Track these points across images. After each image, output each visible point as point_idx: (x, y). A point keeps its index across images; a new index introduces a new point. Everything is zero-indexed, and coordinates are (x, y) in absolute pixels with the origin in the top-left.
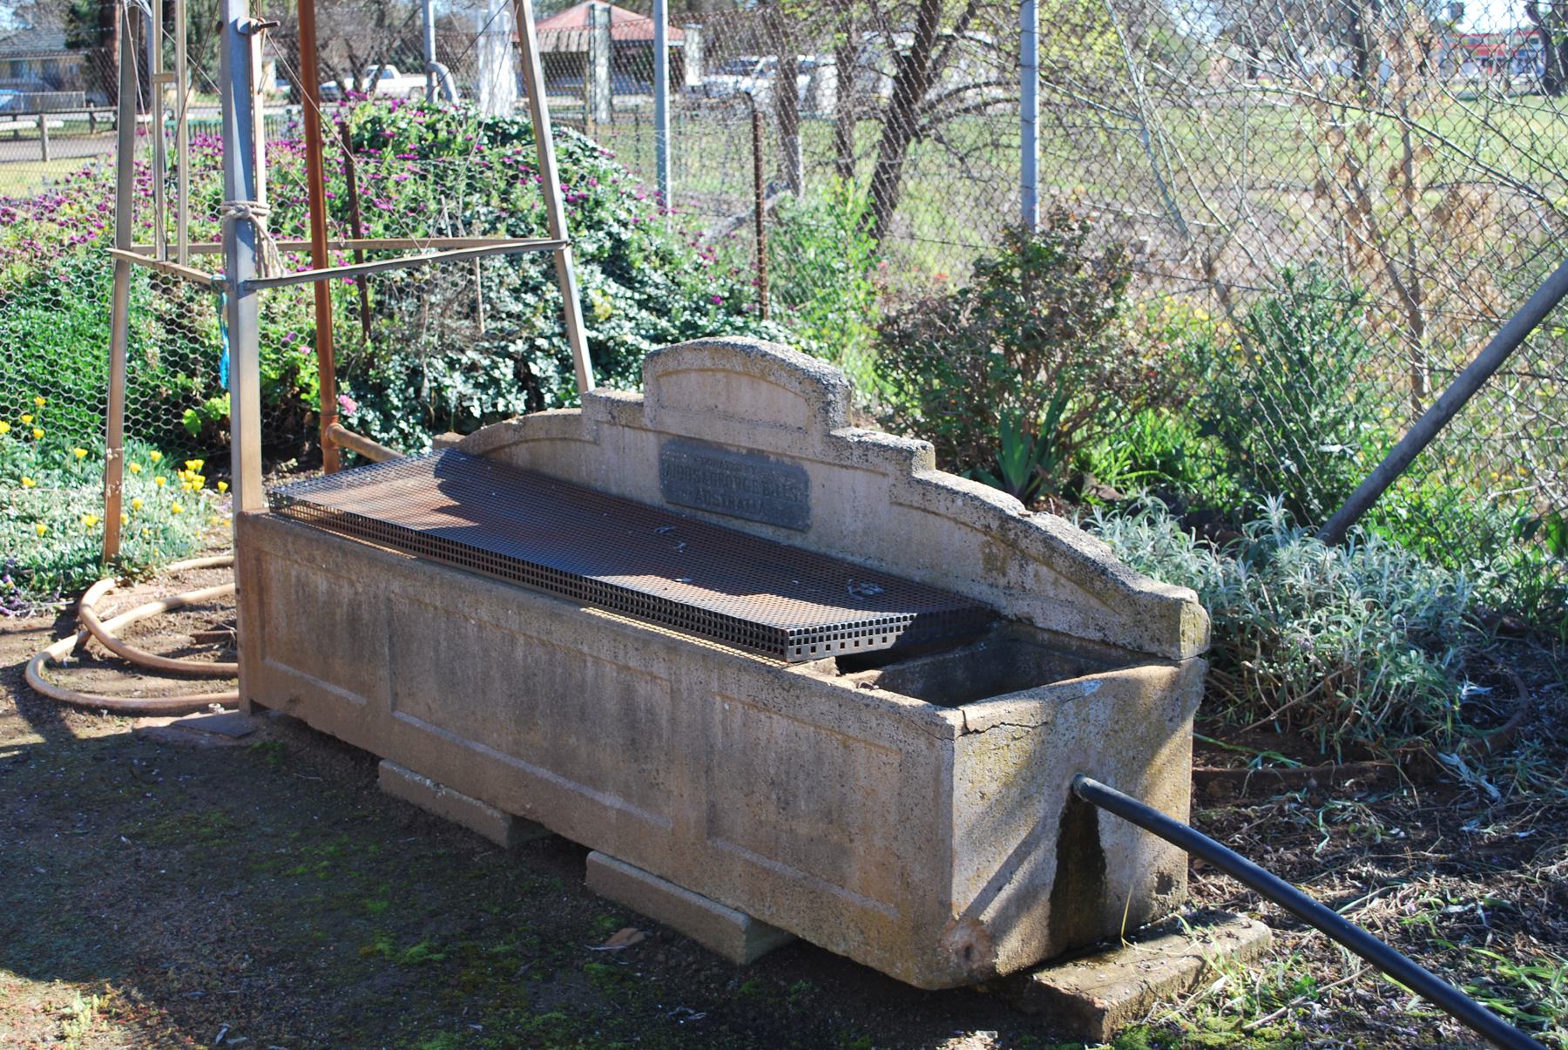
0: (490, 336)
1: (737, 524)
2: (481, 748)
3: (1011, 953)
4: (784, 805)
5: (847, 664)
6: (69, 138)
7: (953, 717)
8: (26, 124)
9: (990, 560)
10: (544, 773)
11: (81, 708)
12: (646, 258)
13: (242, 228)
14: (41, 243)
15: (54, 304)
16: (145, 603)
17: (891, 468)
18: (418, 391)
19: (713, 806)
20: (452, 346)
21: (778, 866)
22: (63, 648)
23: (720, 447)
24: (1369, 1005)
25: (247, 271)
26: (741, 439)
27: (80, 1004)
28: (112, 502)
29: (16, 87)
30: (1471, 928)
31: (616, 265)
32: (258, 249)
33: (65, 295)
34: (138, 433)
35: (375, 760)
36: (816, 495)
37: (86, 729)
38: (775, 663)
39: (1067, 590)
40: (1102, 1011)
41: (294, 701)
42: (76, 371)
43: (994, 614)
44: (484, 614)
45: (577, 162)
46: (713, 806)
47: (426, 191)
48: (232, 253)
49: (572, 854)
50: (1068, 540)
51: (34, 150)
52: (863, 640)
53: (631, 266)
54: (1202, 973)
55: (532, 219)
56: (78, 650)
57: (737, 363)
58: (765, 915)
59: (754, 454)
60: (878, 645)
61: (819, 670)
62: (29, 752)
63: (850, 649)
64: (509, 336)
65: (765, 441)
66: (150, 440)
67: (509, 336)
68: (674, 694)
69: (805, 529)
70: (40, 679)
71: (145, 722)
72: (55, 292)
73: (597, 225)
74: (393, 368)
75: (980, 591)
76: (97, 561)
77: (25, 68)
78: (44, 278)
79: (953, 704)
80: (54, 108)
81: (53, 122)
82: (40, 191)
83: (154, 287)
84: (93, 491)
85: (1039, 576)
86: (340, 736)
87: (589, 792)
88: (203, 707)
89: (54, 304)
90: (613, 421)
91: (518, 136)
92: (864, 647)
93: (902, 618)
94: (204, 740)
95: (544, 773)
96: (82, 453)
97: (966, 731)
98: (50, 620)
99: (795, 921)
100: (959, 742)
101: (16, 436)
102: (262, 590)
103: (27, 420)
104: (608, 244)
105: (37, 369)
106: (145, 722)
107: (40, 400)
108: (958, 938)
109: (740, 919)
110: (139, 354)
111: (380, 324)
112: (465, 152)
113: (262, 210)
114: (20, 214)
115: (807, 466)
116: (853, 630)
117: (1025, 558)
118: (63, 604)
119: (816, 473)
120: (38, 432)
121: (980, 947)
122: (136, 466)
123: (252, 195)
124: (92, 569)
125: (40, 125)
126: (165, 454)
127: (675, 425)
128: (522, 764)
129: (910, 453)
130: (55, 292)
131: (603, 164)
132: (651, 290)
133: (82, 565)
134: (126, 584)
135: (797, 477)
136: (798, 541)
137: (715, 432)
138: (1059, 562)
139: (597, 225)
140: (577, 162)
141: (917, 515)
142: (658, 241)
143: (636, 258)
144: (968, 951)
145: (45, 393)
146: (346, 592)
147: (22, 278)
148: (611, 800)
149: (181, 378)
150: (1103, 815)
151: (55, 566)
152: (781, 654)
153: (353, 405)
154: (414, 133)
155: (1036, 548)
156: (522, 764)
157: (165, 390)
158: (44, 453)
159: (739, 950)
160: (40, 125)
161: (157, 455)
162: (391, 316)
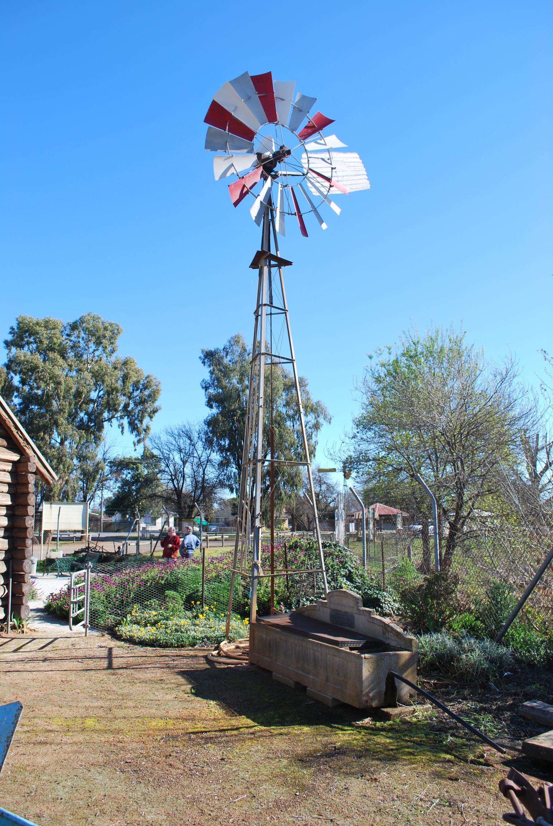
0: (317, 593)
1: (343, 627)
2: (290, 668)
3: (374, 704)
4: (338, 674)
5: (351, 649)
6: (230, 540)
7: (363, 656)
8: (219, 537)
9: (383, 632)
10: (300, 672)
11: (218, 662)
12: (357, 576)
13: (255, 566)
14: (219, 568)
15: (220, 582)
16: (232, 646)
17: (367, 615)
18: (299, 606)
19: (327, 676)
20: (307, 596)
21: (337, 687)
22: (215, 653)
23: (340, 611)
24: (446, 719)
25: (256, 574)
26: (344, 609)
27: (212, 703)
28: (228, 625)
29: (217, 525)
30: (475, 710)
31: (350, 577)
32: (258, 570)
33: (223, 580)
34: (235, 612)
35: (272, 672)
36: (356, 620)
37: (218, 666)
38: (337, 647)
39: (395, 638)
40: (391, 715)
41: (258, 661)
42: (224, 597)
43: (384, 643)
44: (292, 641)
45: (341, 553)
46: (327, 676)
47: (306, 559)
48: (253, 571)
49: (304, 688)
50: (395, 628)
51: (220, 544)
52: (355, 645)
53: (353, 578)
54: (414, 711)
55: (329, 566)
56: (218, 653)
57: (343, 594)
58: (335, 697)
59: (346, 612)
60: (358, 646)
61: (346, 649)
62: (207, 669)
63: (352, 646)
64: (321, 593)
65: (348, 610)
66: (238, 613)
67: (321, 593)
68: (321, 654)
69: (354, 627)
70: (210, 657)
71: (229, 666)
72: (221, 579)
73: (346, 568)
74: (294, 600)
75: (381, 638)
76: (224, 637)
77: (220, 520)
78: (219, 575)
79: (363, 654)
80: (226, 531)
81: (226, 536)
82: (220, 555)
83: (242, 579)
84: (224, 623)
85: (390, 635)
86: (266, 668)
87: (308, 675)
88: (241, 664)
89: (220, 582)
90: (322, 606)
91: (329, 546)
92: (355, 646)
93: (364, 641)
94: (240, 669)
95: (300, 672)
96: (223, 615)
97: (365, 658)
98: (213, 648)
99: (339, 697)
100: (364, 660)
101: (210, 610)
102: (254, 638)
103: (212, 607)
104: (348, 572)
105: (215, 596)
106: (229, 666)
107: (215, 603)
108: (365, 698)
109: (331, 698)
110: (237, 594)
111: (292, 590)
112: (315, 550)
113: (259, 562)
114: (215, 561)
115: (354, 615)
116: (352, 642)
117: (389, 632)
118: (216, 645)
119: (355, 616)
120: (214, 610)
121: (369, 701)
122: (234, 618)
123: (258, 559)
124: (223, 638)
125: (222, 537)
126: (241, 617)
127: (333, 607)
128: (297, 671)
129: (370, 612)
130: (221, 579)
131: (348, 553)
132: (358, 584)
133: (221, 637)
134: (229, 642)
135: (353, 617)
136: (353, 630)
137: (339, 608)
138: (394, 632)
139: (346, 568)
140: (341, 553)
141: (372, 624)
142: (360, 572)
143: (355, 577)
144: (367, 701)
145: (216, 601)
146: (269, 638)
147: (214, 576)
148: (311, 677)
149: (246, 600)
150: (396, 679)
151: (215, 637)
152: (338, 645)
153: (283, 608)
154: (305, 545)
155: (390, 630)
156: (297, 671)
157: (242, 602)
158: (215, 615)
159: (330, 704)
160: (222, 537)
161: (239, 616)
162: (294, 588)
